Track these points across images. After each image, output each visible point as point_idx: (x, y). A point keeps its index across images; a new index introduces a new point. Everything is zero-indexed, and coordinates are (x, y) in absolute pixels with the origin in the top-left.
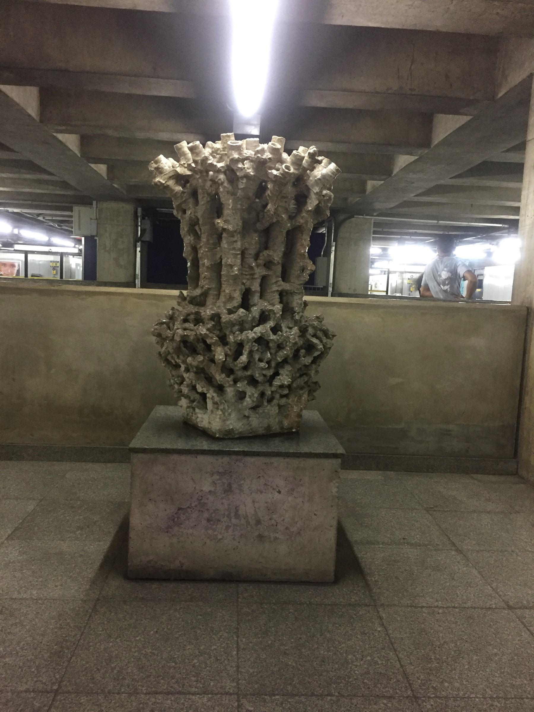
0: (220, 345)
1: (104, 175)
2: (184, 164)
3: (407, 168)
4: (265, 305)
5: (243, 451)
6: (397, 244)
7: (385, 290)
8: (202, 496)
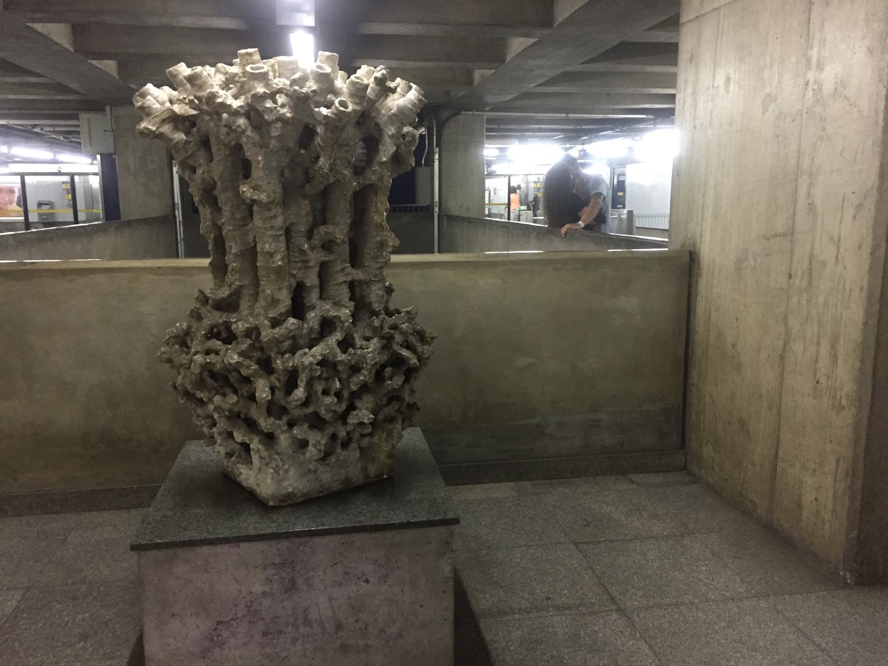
1: (114, 73)
2: (185, 98)
3: (524, 53)
4: (328, 309)
7: (506, 202)
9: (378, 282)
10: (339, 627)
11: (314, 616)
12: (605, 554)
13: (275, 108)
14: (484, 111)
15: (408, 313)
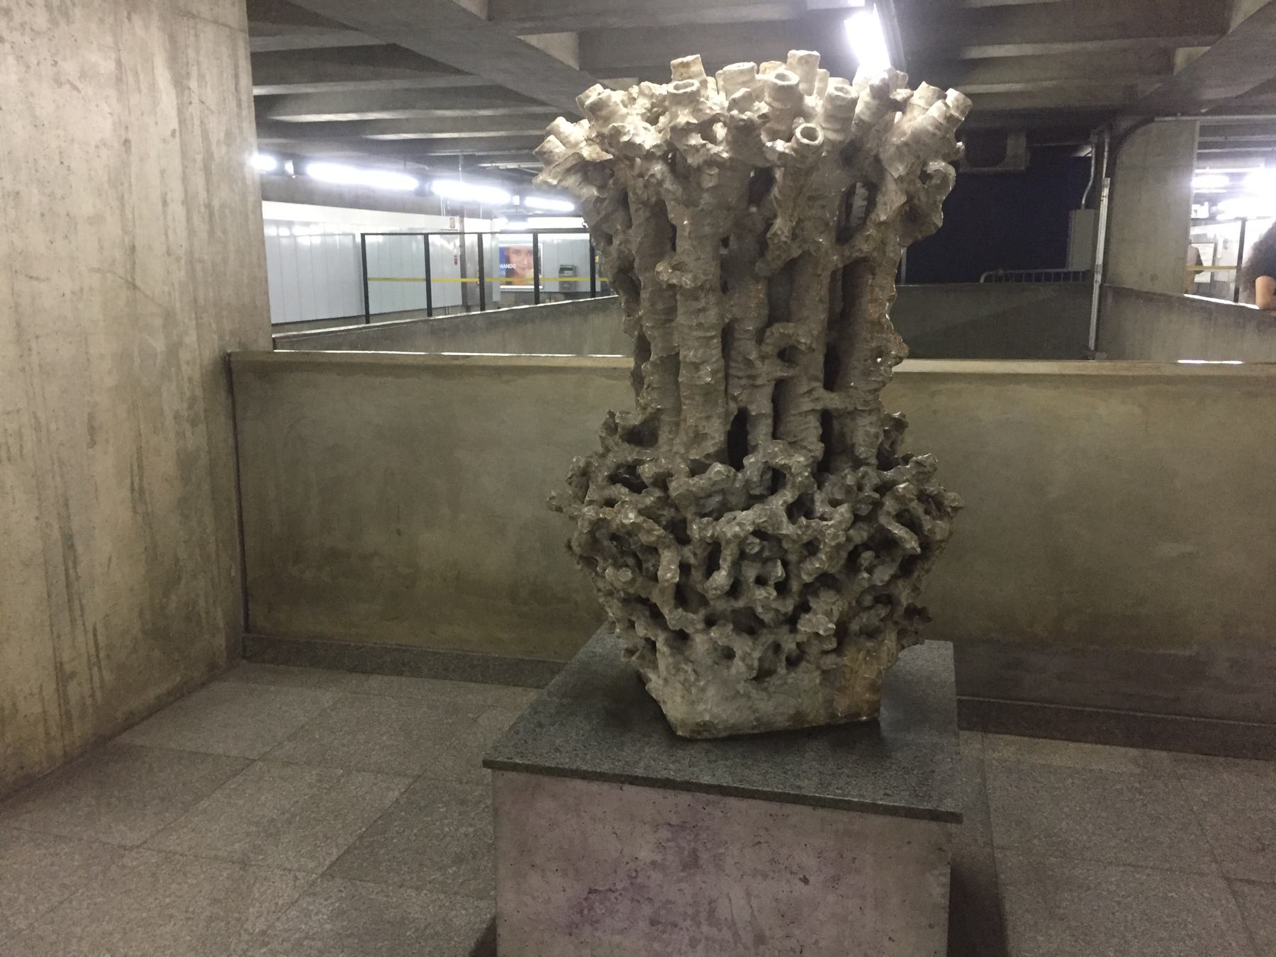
0: (669, 547)
4: (775, 452)
6: (1262, 165)
7: (1235, 264)
9: (870, 412)
10: (760, 939)
11: (723, 912)
14: (1197, 115)
15: (919, 463)
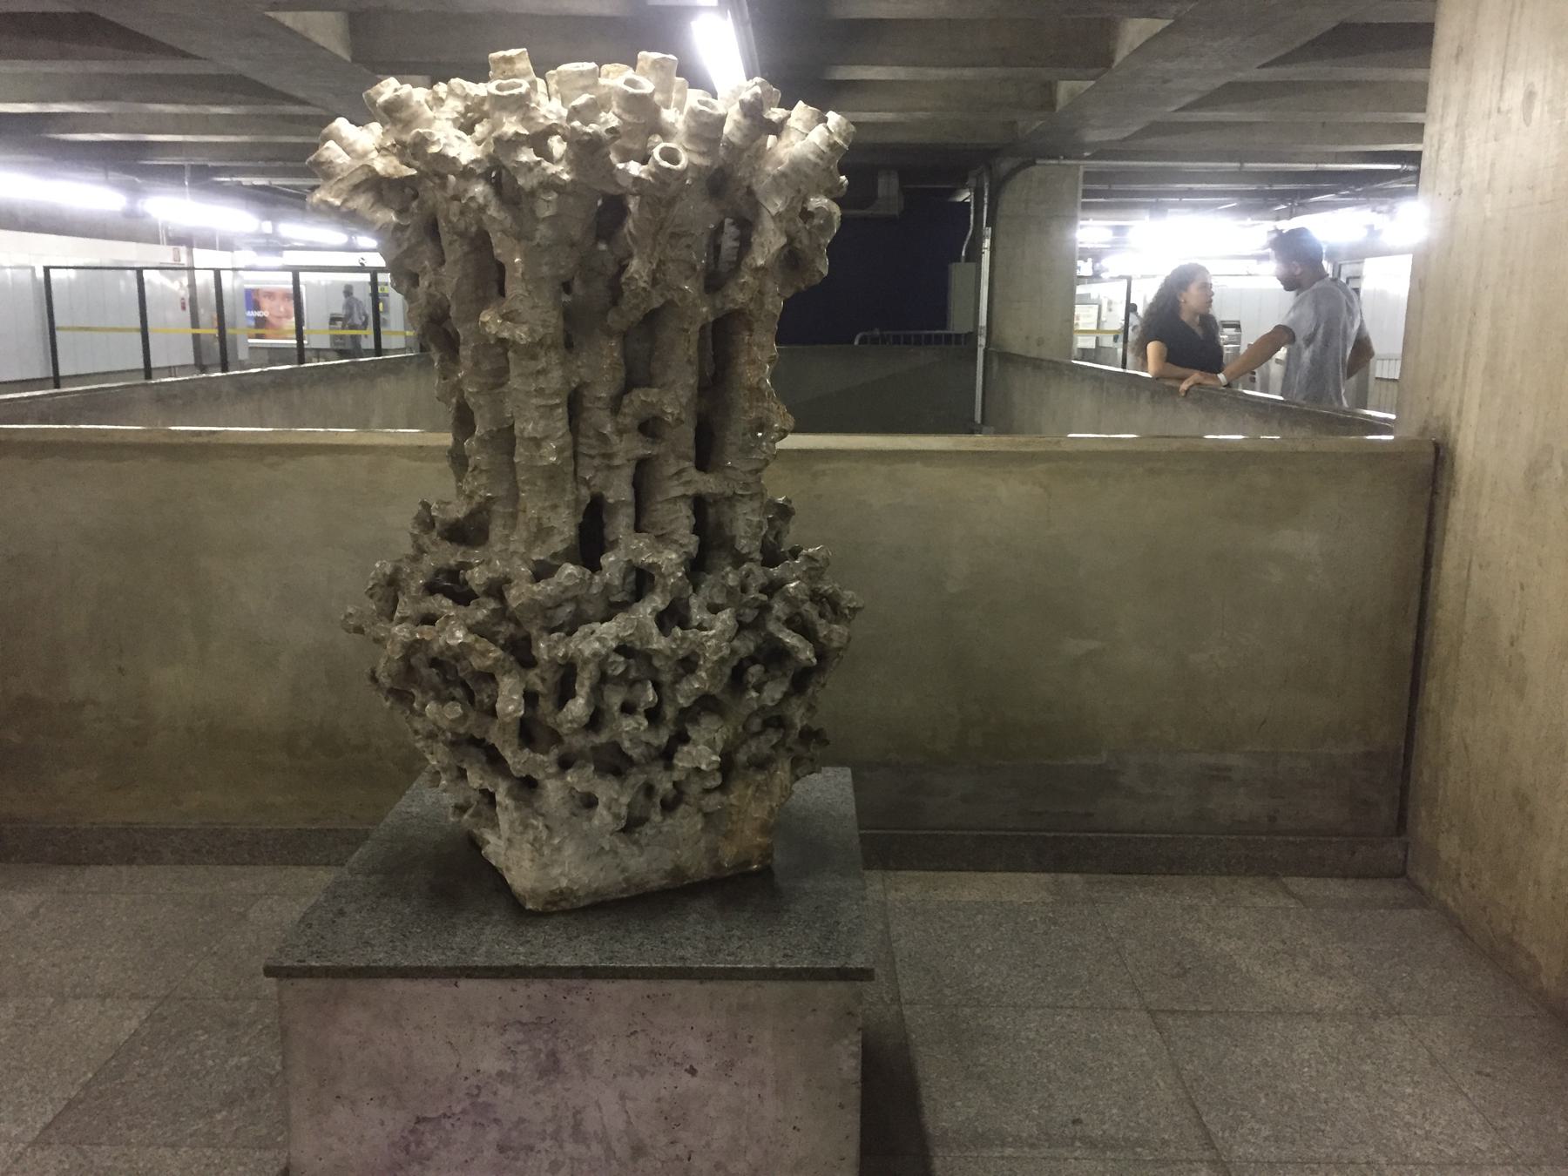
5: (583, 968)
6: (1147, 217)
8: (478, 1087)
9: (752, 497)
10: (638, 1151)
11: (591, 1124)
12: (1209, 1040)
13: (539, 163)
15: (810, 558)
